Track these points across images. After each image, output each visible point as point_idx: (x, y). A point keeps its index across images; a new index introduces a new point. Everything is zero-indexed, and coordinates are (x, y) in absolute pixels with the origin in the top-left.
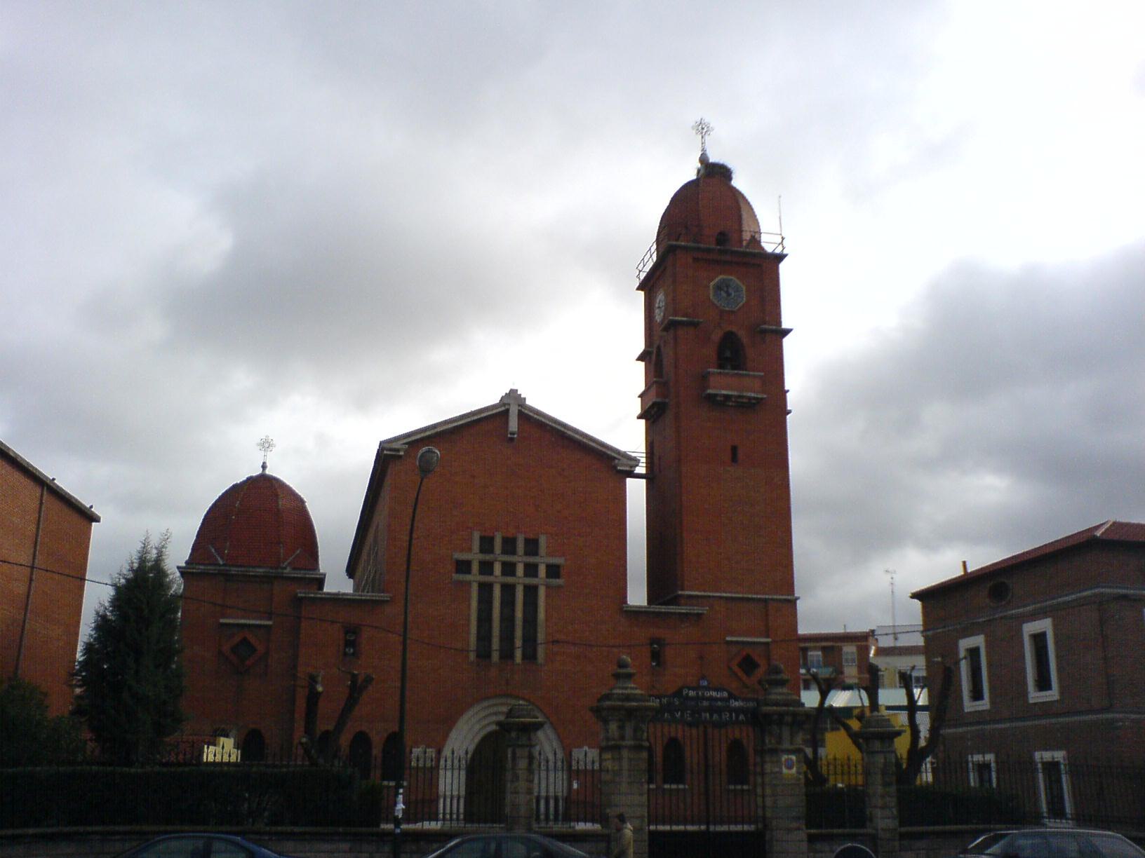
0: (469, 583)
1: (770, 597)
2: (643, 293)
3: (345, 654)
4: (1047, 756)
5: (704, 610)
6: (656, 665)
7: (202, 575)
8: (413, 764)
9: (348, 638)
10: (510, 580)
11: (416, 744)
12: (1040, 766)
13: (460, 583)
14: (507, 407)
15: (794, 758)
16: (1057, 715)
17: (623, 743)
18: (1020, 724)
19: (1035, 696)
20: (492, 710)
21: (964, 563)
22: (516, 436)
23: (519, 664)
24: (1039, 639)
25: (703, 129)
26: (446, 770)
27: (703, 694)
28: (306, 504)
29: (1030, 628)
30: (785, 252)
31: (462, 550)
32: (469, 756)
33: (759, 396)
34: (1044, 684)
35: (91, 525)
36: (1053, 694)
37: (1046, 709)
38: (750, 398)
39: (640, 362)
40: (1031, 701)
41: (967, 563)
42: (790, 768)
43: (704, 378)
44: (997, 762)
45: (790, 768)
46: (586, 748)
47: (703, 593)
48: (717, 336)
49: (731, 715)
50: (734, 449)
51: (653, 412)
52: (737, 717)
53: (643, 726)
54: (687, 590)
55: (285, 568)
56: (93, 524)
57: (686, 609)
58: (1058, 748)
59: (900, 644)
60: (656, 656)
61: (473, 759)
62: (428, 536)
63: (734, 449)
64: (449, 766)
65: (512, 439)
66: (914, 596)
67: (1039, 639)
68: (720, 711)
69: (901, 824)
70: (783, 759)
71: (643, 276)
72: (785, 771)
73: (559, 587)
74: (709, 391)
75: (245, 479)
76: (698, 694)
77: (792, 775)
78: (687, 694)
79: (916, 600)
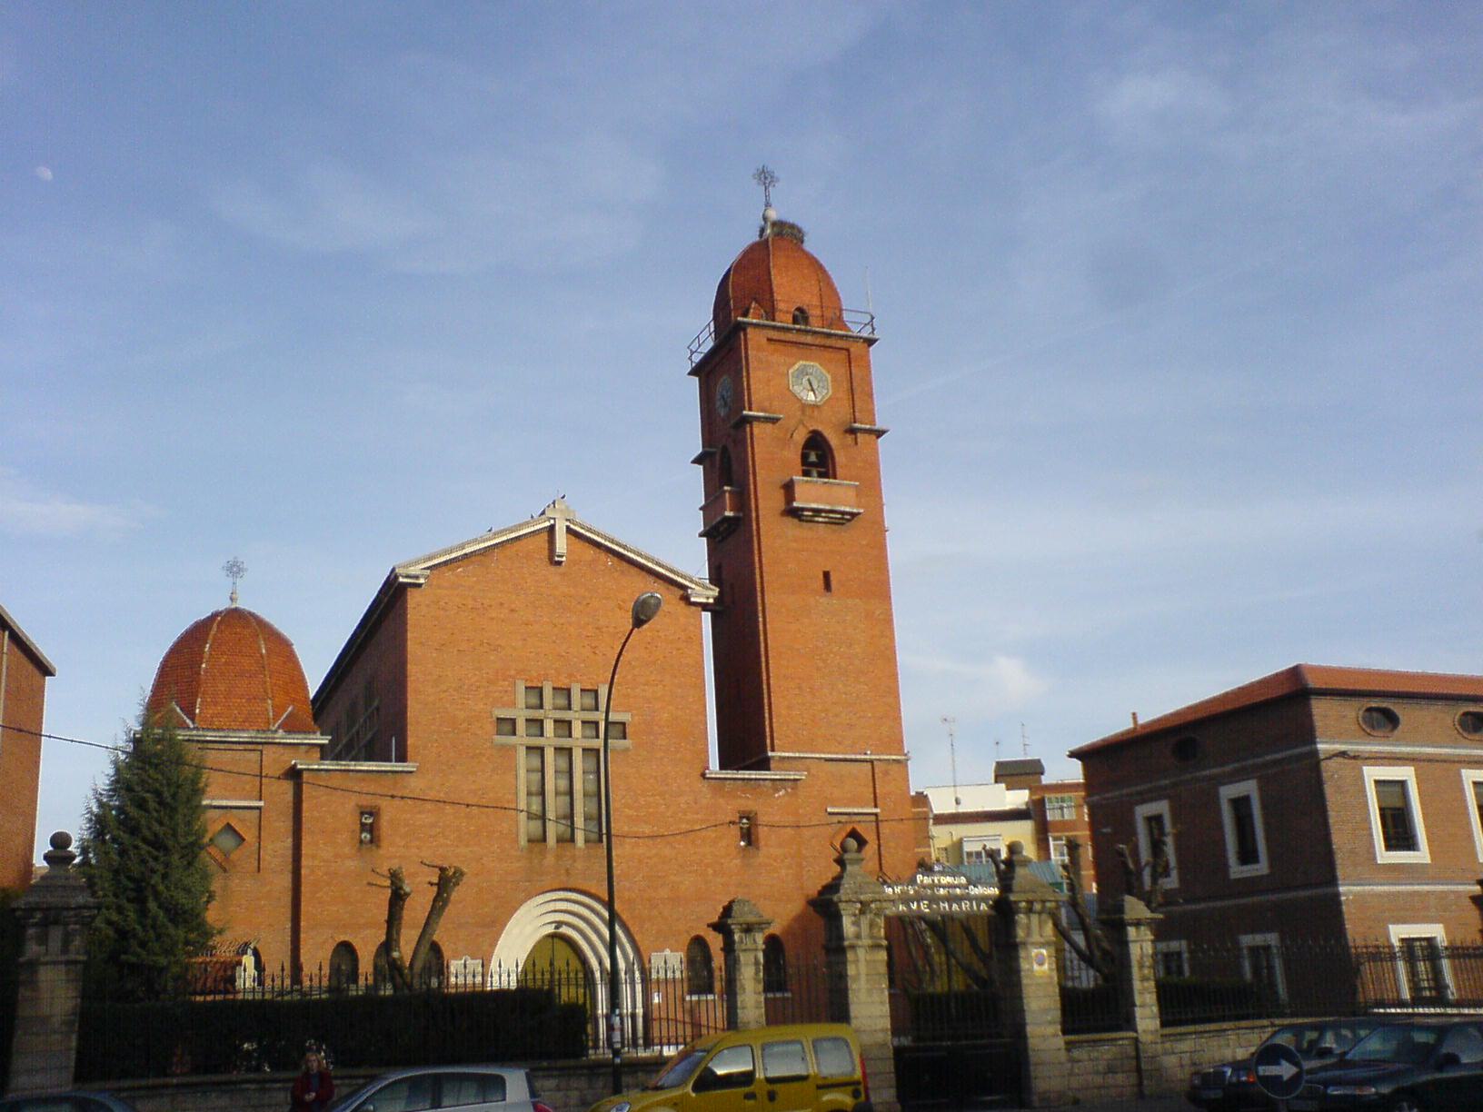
0: (514, 748)
1: (878, 757)
2: (697, 379)
3: (361, 842)
4: (1258, 939)
5: (802, 776)
6: (746, 846)
7: (1036, 773)
8: (453, 980)
9: (363, 820)
10: (565, 742)
11: (457, 957)
12: (1245, 952)
13: (503, 747)
14: (552, 522)
15: (1044, 952)
16: (1262, 892)
17: (860, 943)
18: (1219, 904)
19: (1237, 871)
20: (552, 906)
21: (1134, 714)
22: (564, 559)
23: (580, 849)
24: (1241, 804)
25: (766, 178)
26: (568, 985)
27: (939, 880)
28: (294, 647)
29: (1228, 792)
30: (876, 336)
31: (504, 705)
32: (520, 969)
33: (855, 511)
34: (1248, 855)
35: (45, 679)
36: (1262, 868)
37: (1251, 885)
38: (843, 513)
39: (696, 465)
40: (1233, 876)
41: (1138, 715)
42: (1041, 964)
43: (789, 488)
44: (1191, 952)
45: (1041, 964)
46: (667, 952)
47: (797, 755)
48: (801, 437)
49: (972, 905)
50: (826, 575)
51: (721, 529)
52: (978, 906)
53: (879, 921)
54: (779, 751)
55: (276, 731)
56: (47, 678)
57: (780, 775)
58: (1269, 930)
59: (961, 810)
60: (749, 836)
61: (525, 972)
62: (461, 687)
63: (826, 575)
64: (563, 981)
65: (559, 563)
66: (1073, 755)
67: (1241, 804)
68: (959, 899)
69: (1164, 1024)
70: (1033, 954)
71: (697, 358)
72: (1036, 967)
73: (627, 750)
74: (795, 504)
75: (209, 614)
76: (933, 881)
77: (1044, 972)
78: (922, 881)
79: (1075, 760)
